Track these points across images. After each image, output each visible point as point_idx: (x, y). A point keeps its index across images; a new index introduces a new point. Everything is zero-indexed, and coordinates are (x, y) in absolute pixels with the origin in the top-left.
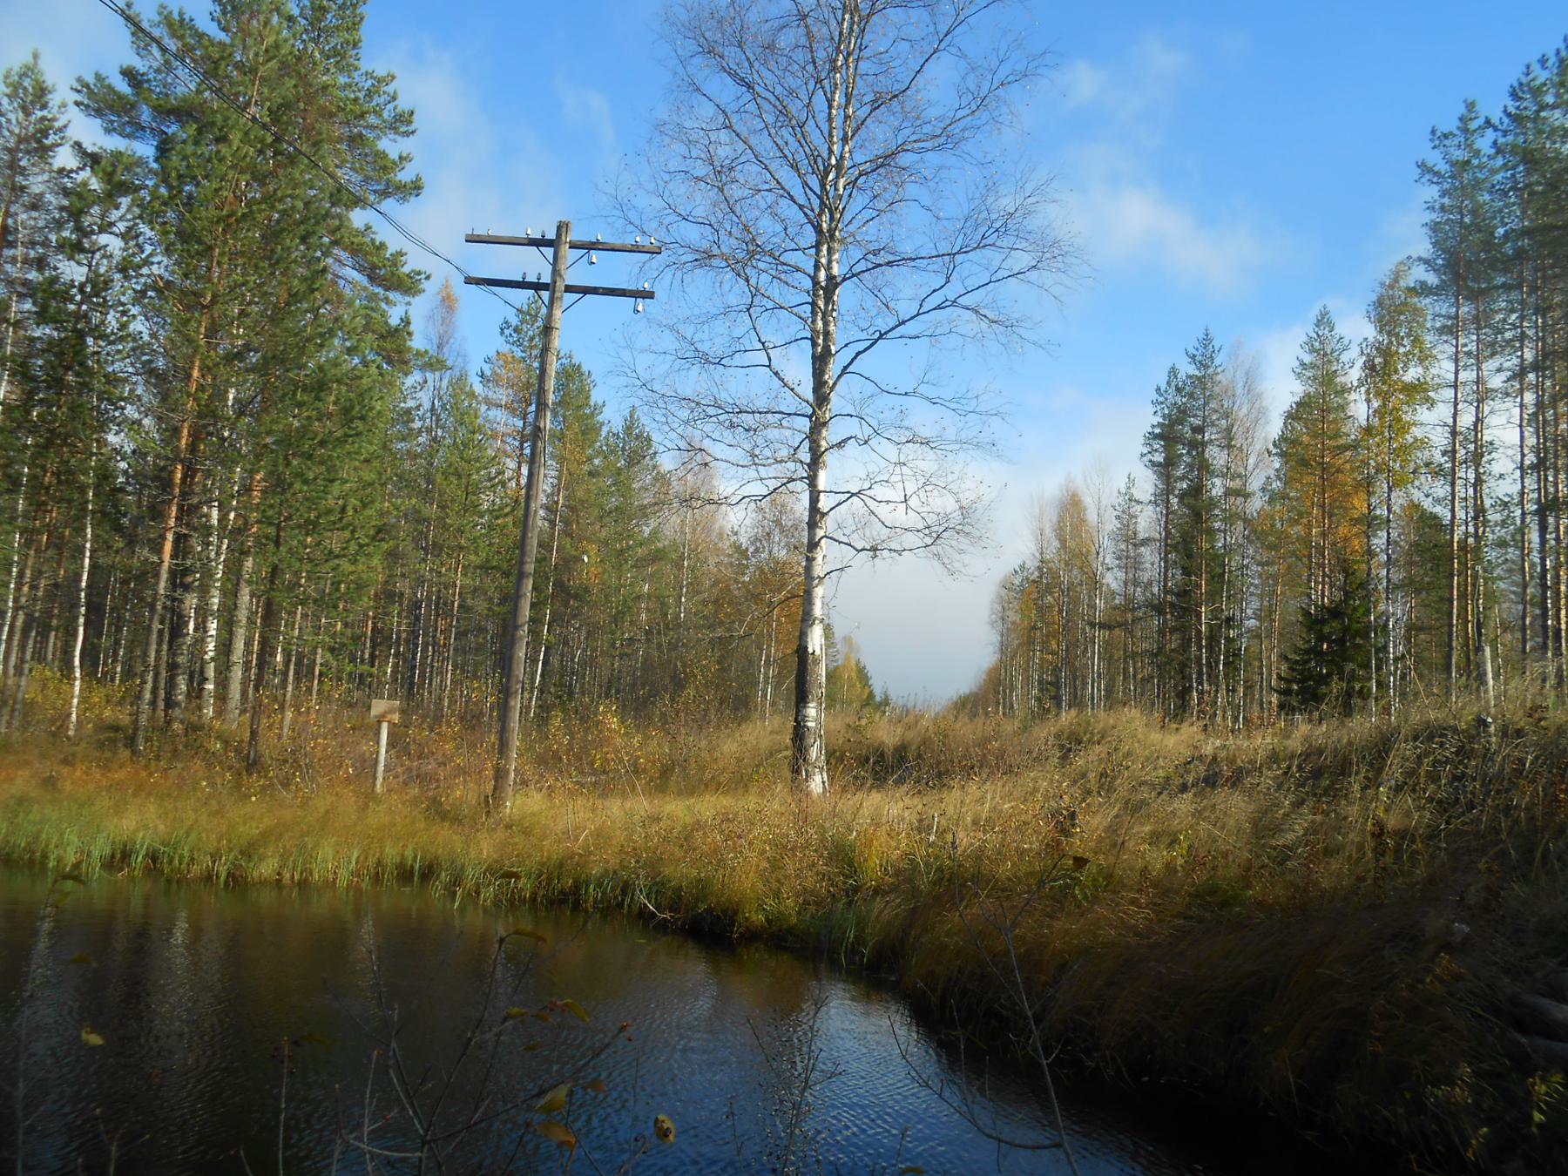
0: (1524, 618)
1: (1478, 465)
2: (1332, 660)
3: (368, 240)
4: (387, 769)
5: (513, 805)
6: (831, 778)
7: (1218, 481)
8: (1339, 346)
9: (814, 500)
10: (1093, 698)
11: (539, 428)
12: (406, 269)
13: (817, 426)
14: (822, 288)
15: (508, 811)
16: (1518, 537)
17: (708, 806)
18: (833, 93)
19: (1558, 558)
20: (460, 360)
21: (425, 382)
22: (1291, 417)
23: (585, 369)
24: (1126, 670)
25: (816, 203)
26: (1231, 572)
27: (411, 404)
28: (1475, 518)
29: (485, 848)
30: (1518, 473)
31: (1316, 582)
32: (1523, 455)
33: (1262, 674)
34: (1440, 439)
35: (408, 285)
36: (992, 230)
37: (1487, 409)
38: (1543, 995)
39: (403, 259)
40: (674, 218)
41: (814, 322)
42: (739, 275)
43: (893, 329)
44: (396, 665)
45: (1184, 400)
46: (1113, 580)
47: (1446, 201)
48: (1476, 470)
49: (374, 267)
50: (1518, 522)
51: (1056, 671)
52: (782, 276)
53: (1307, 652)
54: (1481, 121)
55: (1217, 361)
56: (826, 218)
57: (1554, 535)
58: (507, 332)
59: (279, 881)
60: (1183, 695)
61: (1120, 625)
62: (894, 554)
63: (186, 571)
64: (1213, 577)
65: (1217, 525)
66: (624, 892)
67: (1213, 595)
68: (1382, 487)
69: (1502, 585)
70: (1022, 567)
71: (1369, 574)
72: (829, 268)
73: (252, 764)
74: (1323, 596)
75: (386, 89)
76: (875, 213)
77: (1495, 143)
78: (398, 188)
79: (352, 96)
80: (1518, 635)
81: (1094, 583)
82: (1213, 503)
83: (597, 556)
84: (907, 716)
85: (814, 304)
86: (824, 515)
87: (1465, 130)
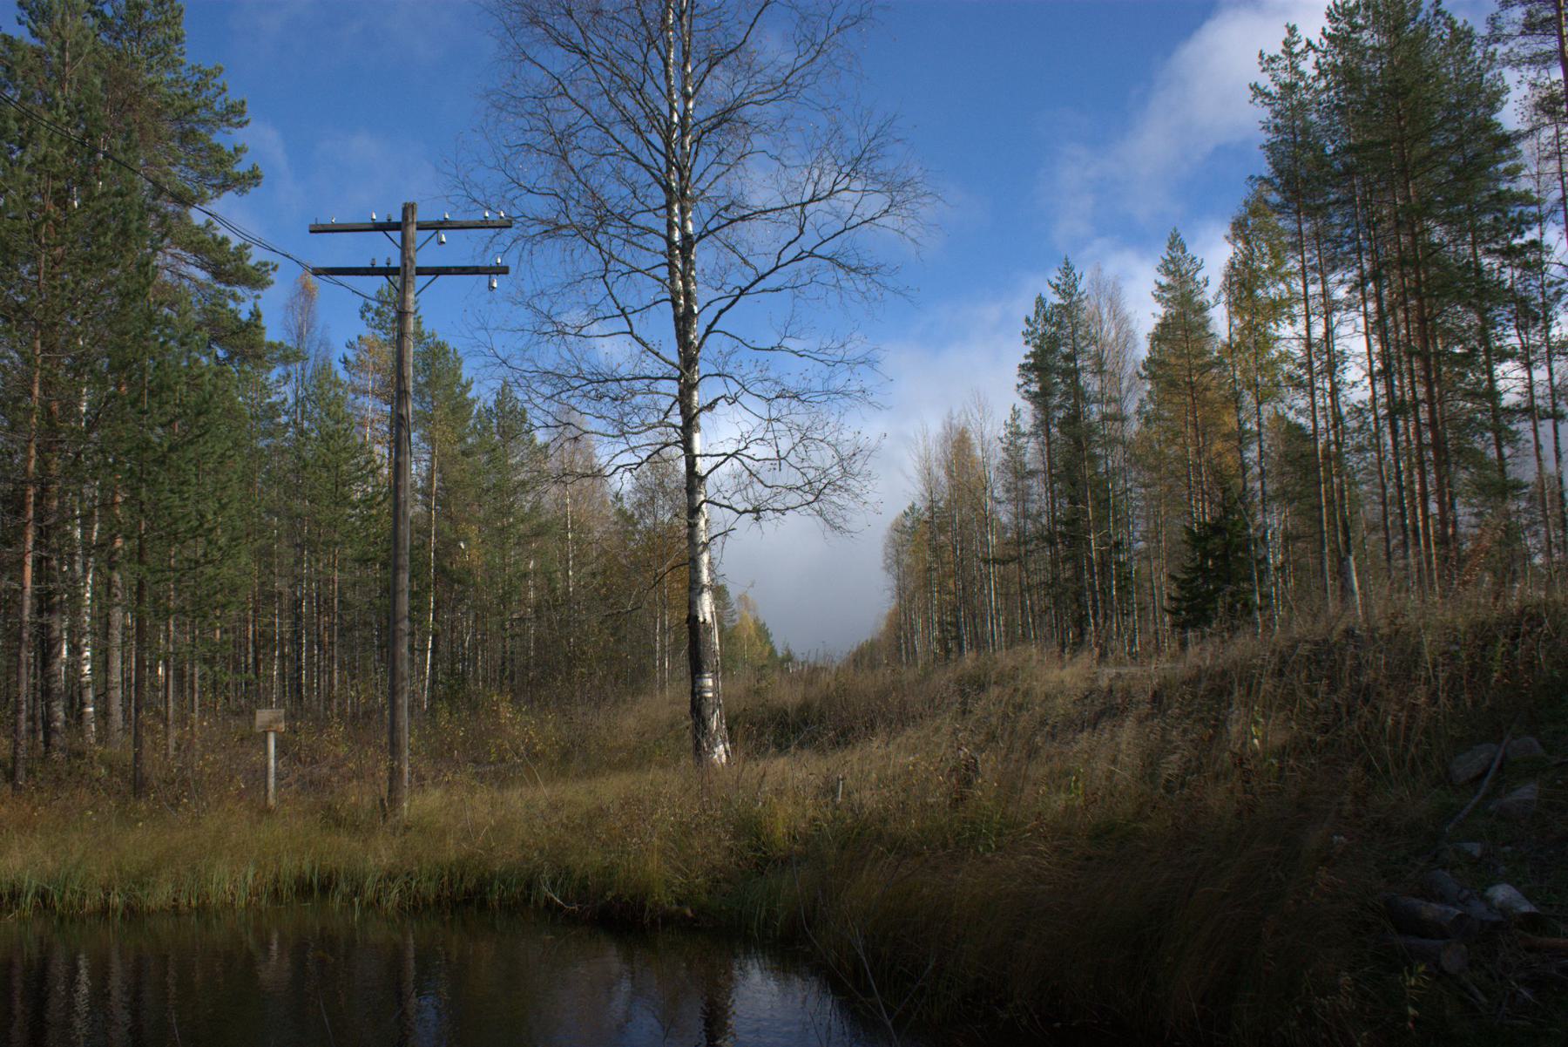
0: (1385, 518)
1: (1332, 375)
2: (1217, 576)
3: (209, 237)
4: (278, 776)
5: (411, 805)
6: (734, 749)
7: (1095, 408)
8: (1193, 266)
9: (691, 464)
10: (993, 635)
11: (401, 416)
12: (252, 262)
13: (687, 389)
14: (678, 248)
15: (406, 813)
16: (1374, 441)
17: (611, 788)
18: (668, 52)
19: (1410, 459)
20: (322, 349)
21: (289, 375)
22: (1158, 338)
23: (451, 347)
24: (1023, 603)
25: (662, 161)
26: (1115, 496)
27: (274, 398)
28: (1335, 426)
29: (380, 855)
30: (1367, 381)
31: (1197, 501)
32: (1371, 362)
33: (1153, 595)
34: (1297, 349)
35: (255, 279)
36: (842, 176)
37: (1335, 320)
38: (1415, 896)
39: (248, 251)
40: (517, 192)
41: (673, 282)
42: (589, 241)
43: (752, 284)
44: (282, 667)
45: (1053, 329)
46: (1004, 515)
47: (1278, 121)
48: (1332, 380)
49: (217, 264)
50: (1373, 427)
51: (955, 610)
52: (634, 239)
53: (1194, 570)
54: (1302, 45)
55: (1080, 289)
56: (674, 176)
57: (1404, 438)
58: (369, 315)
59: (176, 907)
60: (1080, 623)
61: (1012, 559)
62: (778, 514)
63: (50, 594)
64: (1099, 504)
65: (1098, 451)
66: (529, 886)
67: (1101, 521)
68: (1249, 399)
69: (1365, 487)
70: (912, 508)
71: (1244, 489)
72: (683, 228)
73: (139, 786)
74: (1204, 512)
75: (214, 82)
76: (723, 169)
77: (1317, 63)
78: (237, 180)
79: (180, 92)
80: (1382, 535)
81: (986, 520)
82: (1091, 429)
83: (478, 537)
84: (813, 673)
85: (671, 265)
86: (702, 479)
87: (1290, 54)
